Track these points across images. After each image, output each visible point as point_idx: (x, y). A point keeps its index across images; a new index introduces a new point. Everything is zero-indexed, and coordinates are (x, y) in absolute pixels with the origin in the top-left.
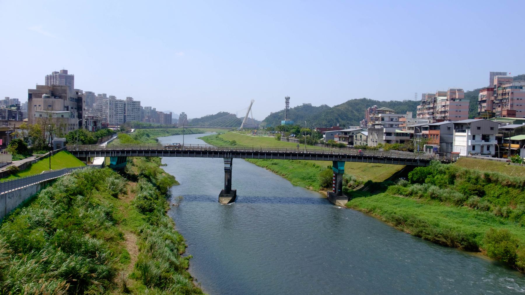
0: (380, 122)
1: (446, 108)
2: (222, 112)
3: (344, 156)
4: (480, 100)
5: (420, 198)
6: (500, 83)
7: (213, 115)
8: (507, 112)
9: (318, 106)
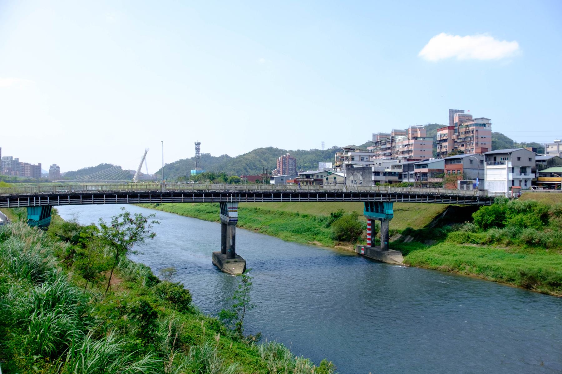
0: (351, 162)
1: (409, 147)
2: (104, 164)
3: (393, 195)
4: (438, 139)
5: (507, 246)
6: (461, 121)
7: (92, 168)
8: (481, 150)
9: (218, 156)
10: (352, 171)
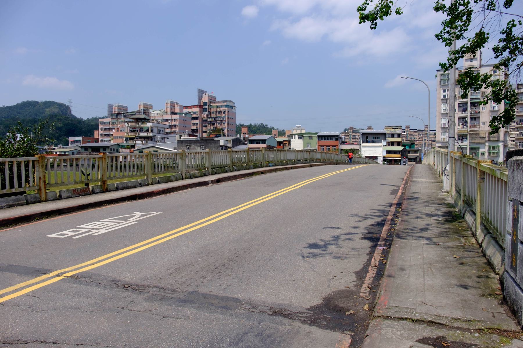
10: (187, 144)
